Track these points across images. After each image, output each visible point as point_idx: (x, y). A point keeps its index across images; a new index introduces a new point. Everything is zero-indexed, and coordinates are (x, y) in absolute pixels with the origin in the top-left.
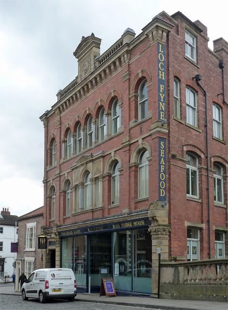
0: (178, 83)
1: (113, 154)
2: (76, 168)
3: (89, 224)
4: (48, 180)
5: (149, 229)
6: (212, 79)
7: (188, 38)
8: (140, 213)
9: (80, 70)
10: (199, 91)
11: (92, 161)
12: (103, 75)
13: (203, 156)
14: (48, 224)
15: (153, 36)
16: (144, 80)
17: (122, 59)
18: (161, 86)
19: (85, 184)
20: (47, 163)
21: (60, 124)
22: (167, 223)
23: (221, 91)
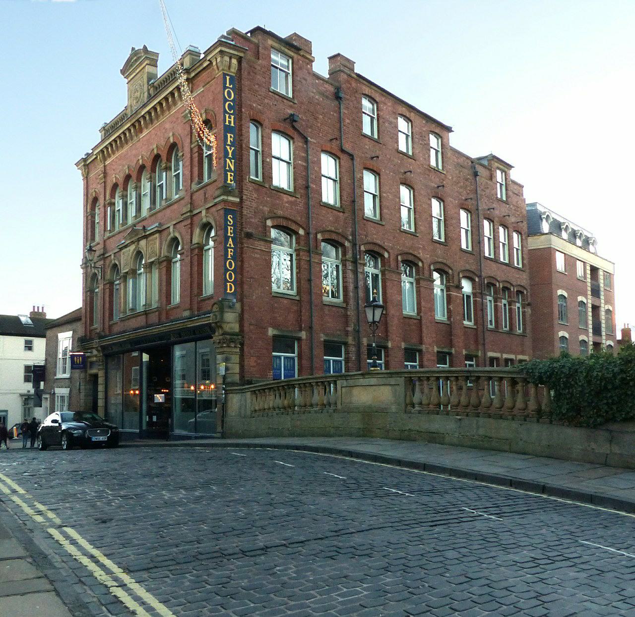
0: (260, 129)
2: (126, 246)
3: (141, 333)
6: (321, 117)
7: (278, 59)
8: (202, 316)
10: (296, 136)
11: (146, 237)
15: (217, 63)
18: (229, 135)
20: (87, 236)
23: (337, 134)
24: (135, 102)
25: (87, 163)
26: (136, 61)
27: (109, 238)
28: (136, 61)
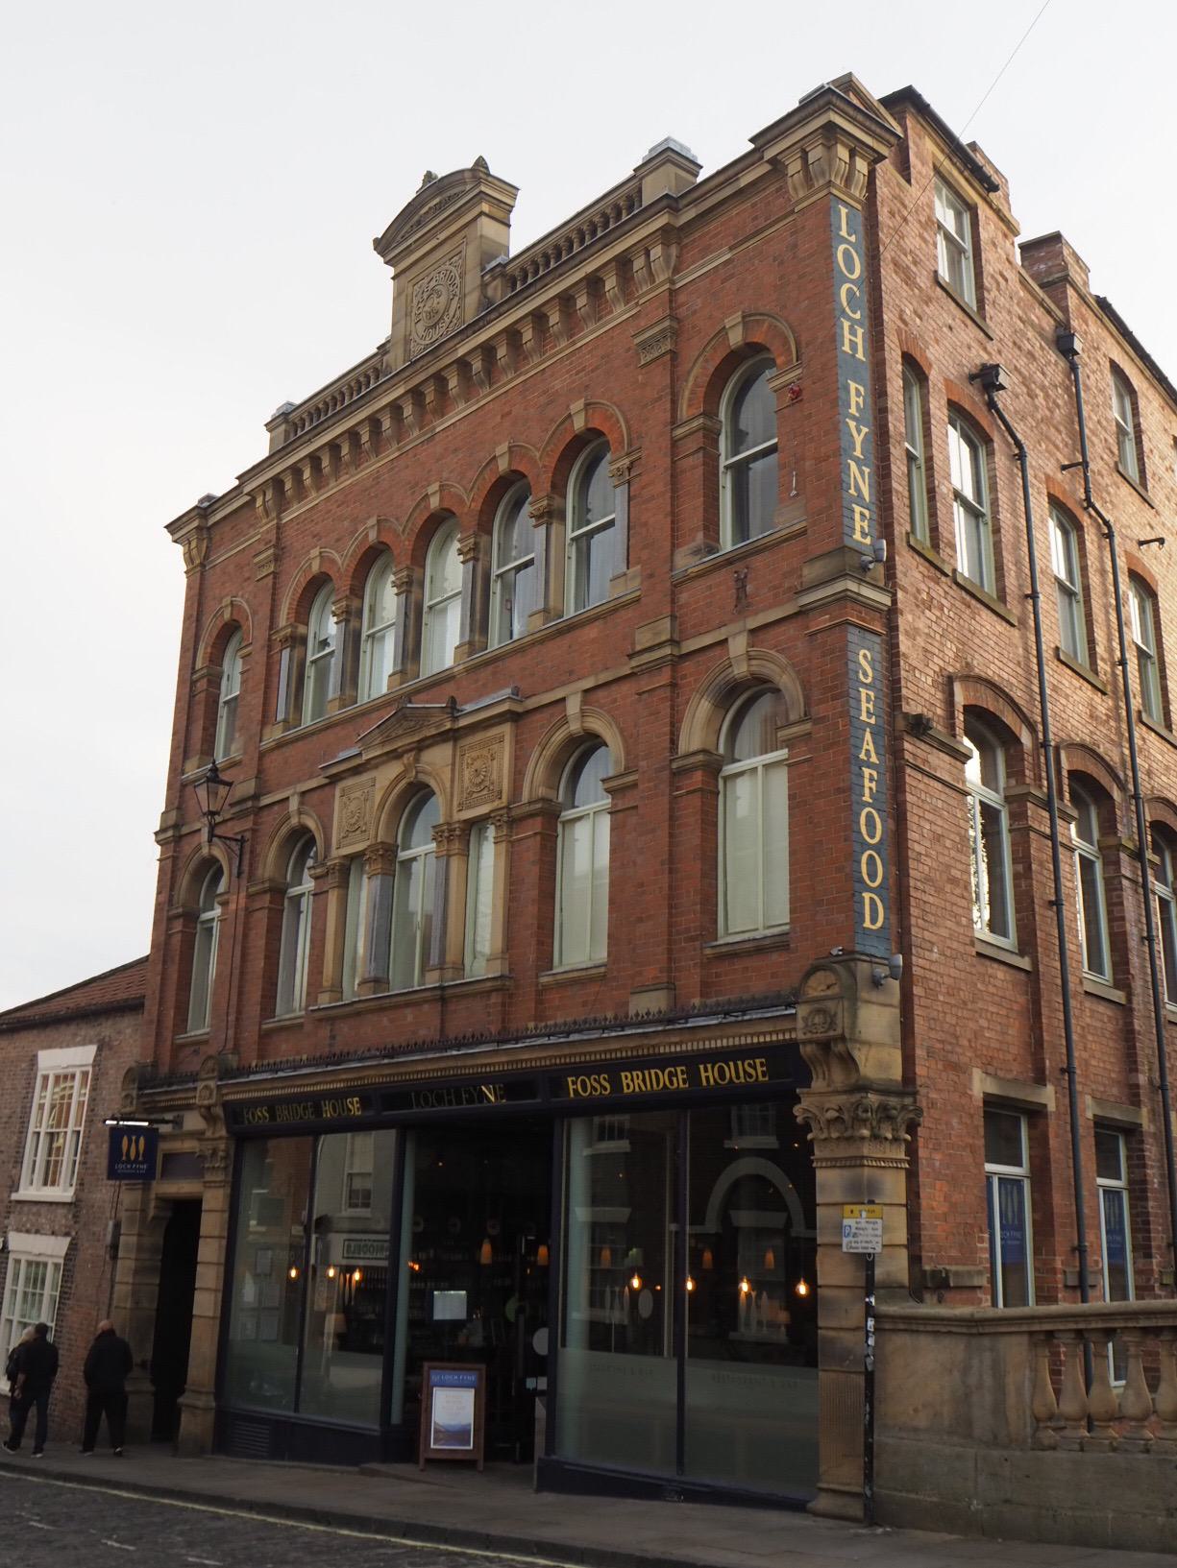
1: (573, 706)
2: (356, 771)
4: (185, 830)
5: (797, 1110)
9: (404, 308)
11: (453, 736)
12: (325, 462)
13: (1026, 739)
14: (166, 1057)
16: (518, 485)
17: (638, 263)
19: (403, 855)
21: (277, 558)
22: (897, 1073)
24: (420, 327)
25: (211, 522)
26: (439, 208)
27: (280, 745)
28: (439, 208)
